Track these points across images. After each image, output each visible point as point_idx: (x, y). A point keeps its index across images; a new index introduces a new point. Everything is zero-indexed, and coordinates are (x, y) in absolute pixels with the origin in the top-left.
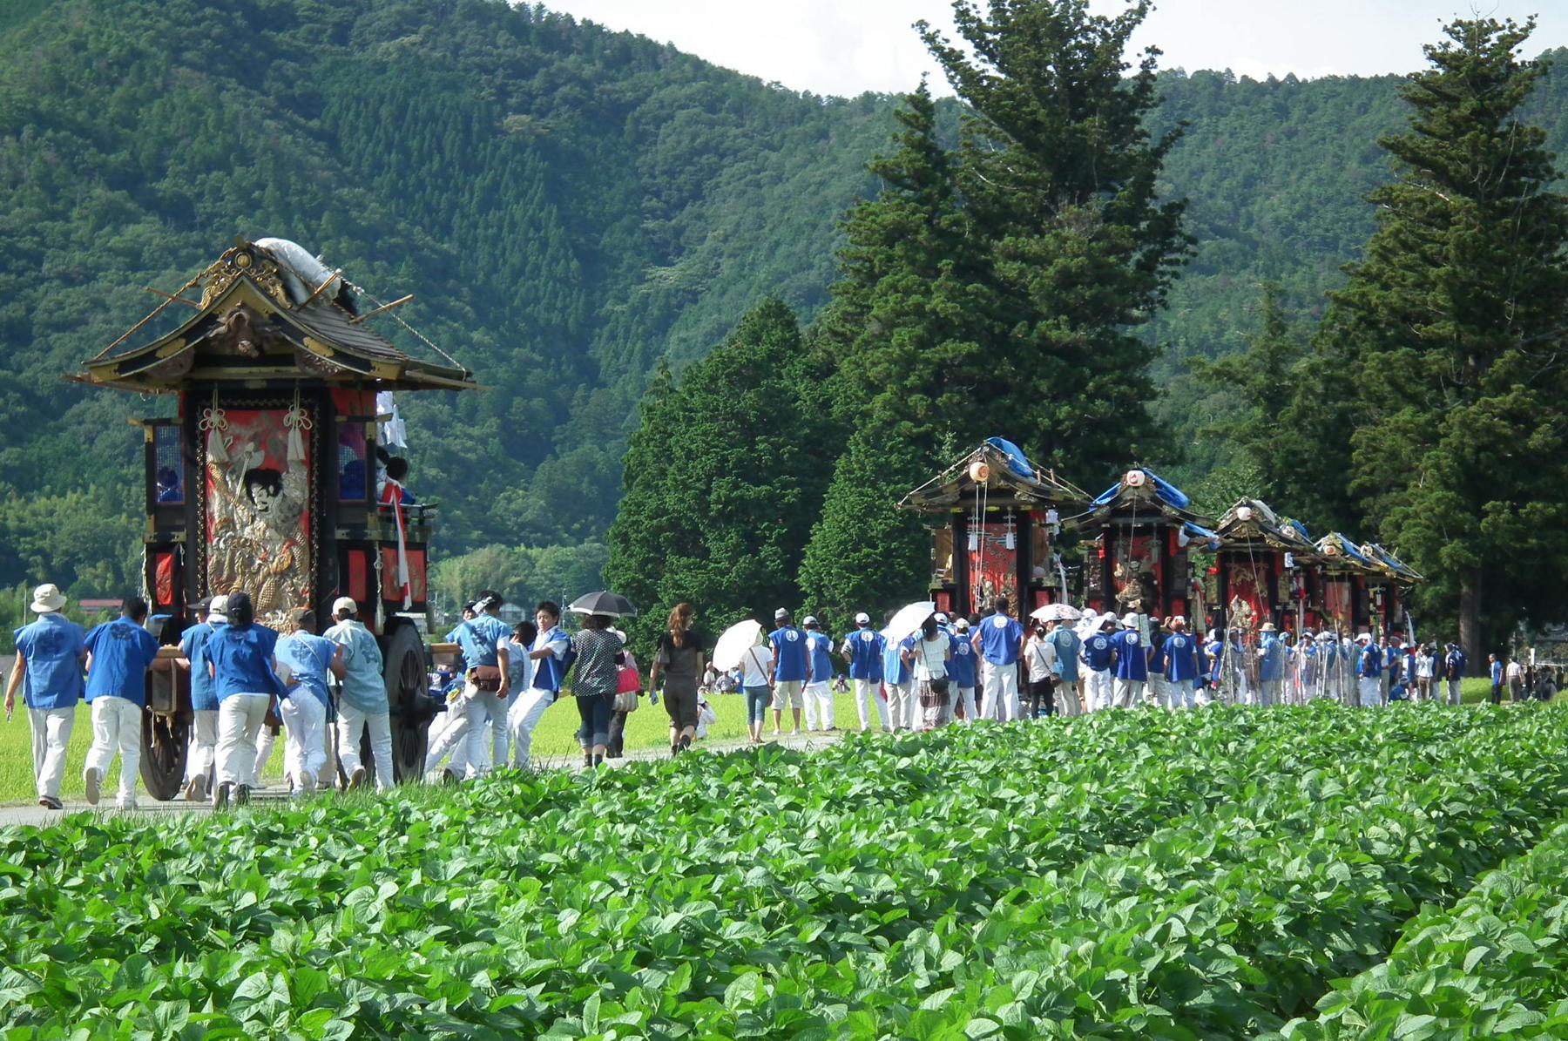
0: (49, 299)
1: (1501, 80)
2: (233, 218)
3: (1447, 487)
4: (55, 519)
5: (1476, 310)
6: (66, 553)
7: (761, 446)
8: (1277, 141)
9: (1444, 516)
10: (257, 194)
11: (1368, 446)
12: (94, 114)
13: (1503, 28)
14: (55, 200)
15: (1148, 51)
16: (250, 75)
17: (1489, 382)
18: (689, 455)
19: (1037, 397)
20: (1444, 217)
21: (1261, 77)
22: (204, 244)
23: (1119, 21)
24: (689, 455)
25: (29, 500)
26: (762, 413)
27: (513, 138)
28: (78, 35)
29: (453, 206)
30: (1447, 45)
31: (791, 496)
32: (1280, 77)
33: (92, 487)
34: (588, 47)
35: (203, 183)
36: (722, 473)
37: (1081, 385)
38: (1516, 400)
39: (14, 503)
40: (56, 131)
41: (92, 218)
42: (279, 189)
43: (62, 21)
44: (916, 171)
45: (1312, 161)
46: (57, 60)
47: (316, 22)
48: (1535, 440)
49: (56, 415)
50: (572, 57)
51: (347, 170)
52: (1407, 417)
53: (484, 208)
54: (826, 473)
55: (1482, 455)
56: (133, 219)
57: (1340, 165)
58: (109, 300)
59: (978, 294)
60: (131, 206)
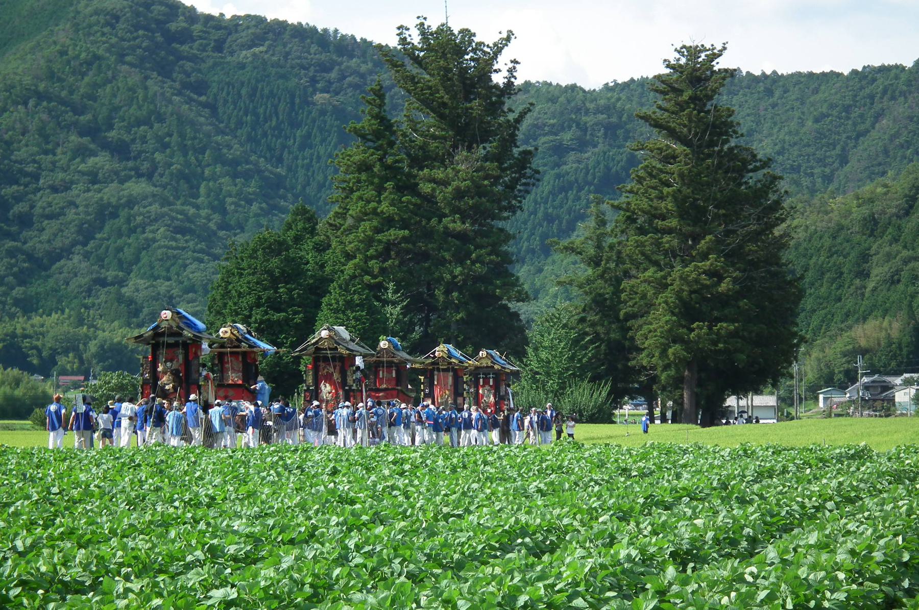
0: (43, 201)
1: (707, 79)
2: (153, 154)
3: (673, 314)
4: (45, 329)
5: (692, 213)
6: (51, 348)
7: (281, 290)
8: (766, 110)
9: (670, 330)
10: (167, 139)
11: (631, 290)
12: (71, 93)
13: (709, 50)
14: (47, 143)
15: (512, 62)
16: (165, 71)
17: (698, 254)
18: (240, 295)
19: (443, 262)
20: (670, 158)
21: (757, 73)
22: (136, 169)
23: (495, 45)
24: (240, 295)
25: (29, 318)
26: (283, 272)
27: (319, 107)
28: (63, 46)
29: (284, 147)
30: (678, 60)
31: (298, 319)
32: (768, 72)
33: (67, 311)
34: (364, 54)
35: (136, 133)
36: (258, 305)
37: (468, 255)
38: (712, 264)
39: (20, 320)
40: (49, 102)
41: (69, 153)
42: (180, 136)
43: (54, 38)
44: (374, 131)
45: (786, 121)
46: (50, 61)
47: (205, 39)
48: (723, 287)
49: (46, 269)
50: (354, 60)
51: (222, 125)
52: (650, 274)
53: (302, 148)
54: (318, 306)
55: (693, 296)
56: (94, 154)
57: (802, 124)
58: (78, 201)
59: (409, 202)
60: (92, 146)
